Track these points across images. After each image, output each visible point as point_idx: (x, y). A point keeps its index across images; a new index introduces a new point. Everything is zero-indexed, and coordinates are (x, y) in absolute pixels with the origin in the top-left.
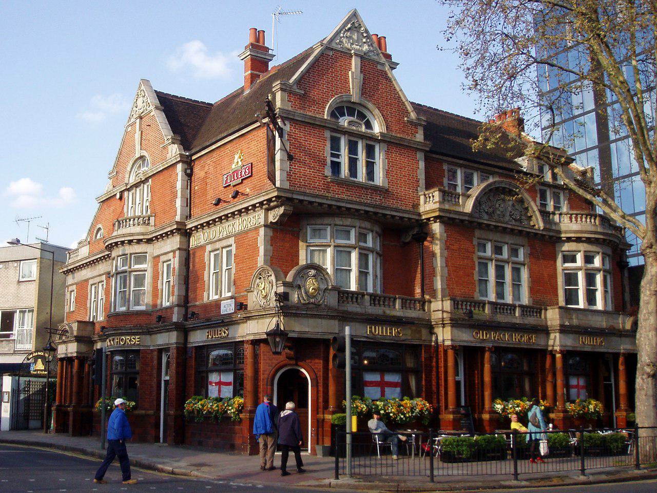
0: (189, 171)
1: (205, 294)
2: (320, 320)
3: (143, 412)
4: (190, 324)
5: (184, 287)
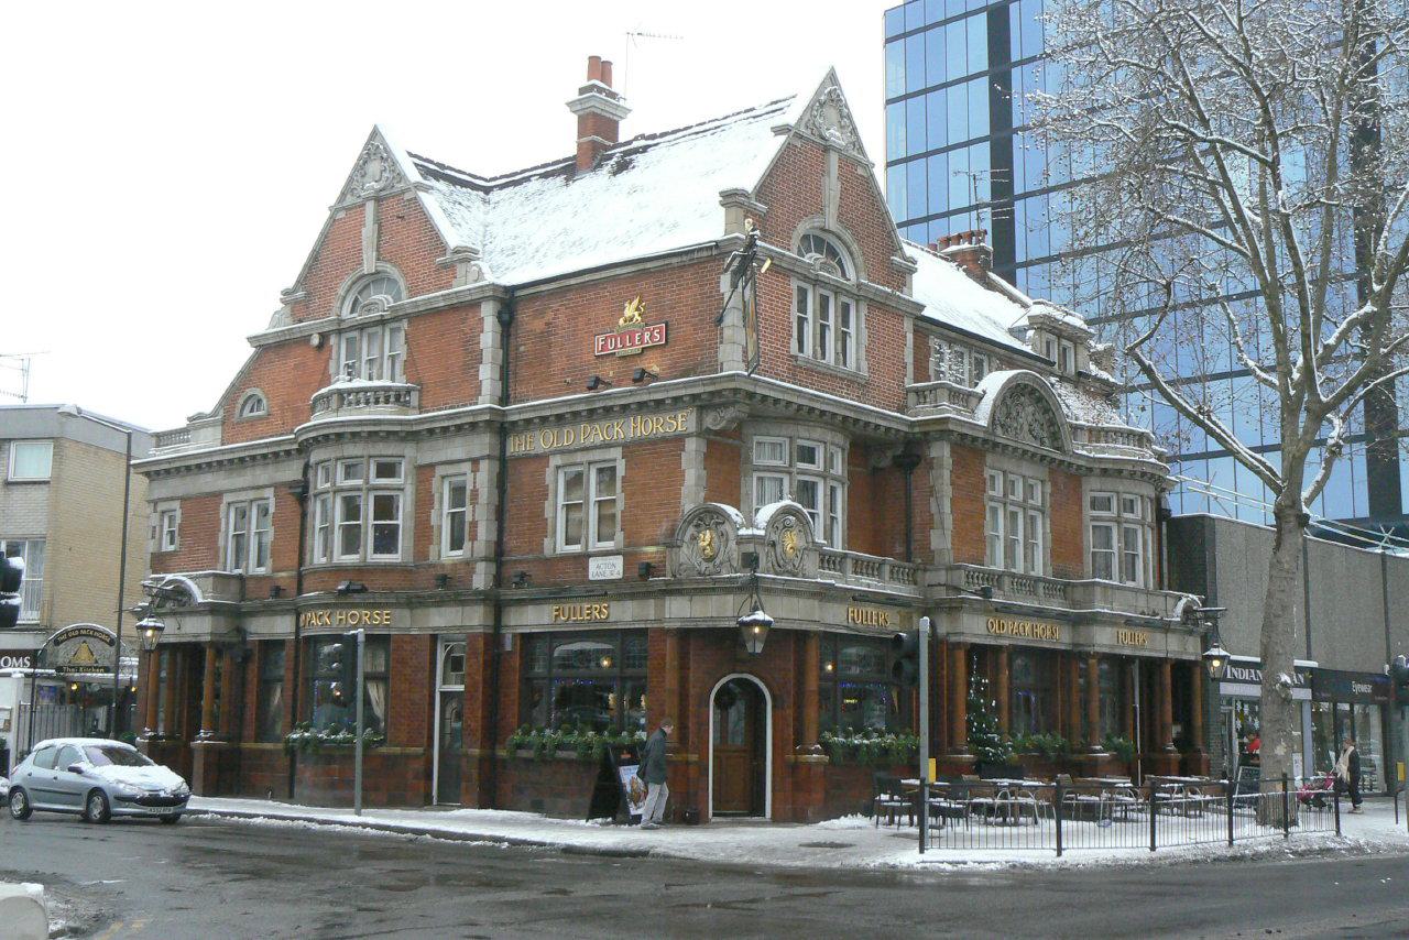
0: (506, 317)
1: (547, 541)
2: (796, 600)
3: (398, 750)
4: (510, 593)
5: (494, 526)
